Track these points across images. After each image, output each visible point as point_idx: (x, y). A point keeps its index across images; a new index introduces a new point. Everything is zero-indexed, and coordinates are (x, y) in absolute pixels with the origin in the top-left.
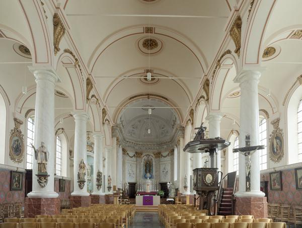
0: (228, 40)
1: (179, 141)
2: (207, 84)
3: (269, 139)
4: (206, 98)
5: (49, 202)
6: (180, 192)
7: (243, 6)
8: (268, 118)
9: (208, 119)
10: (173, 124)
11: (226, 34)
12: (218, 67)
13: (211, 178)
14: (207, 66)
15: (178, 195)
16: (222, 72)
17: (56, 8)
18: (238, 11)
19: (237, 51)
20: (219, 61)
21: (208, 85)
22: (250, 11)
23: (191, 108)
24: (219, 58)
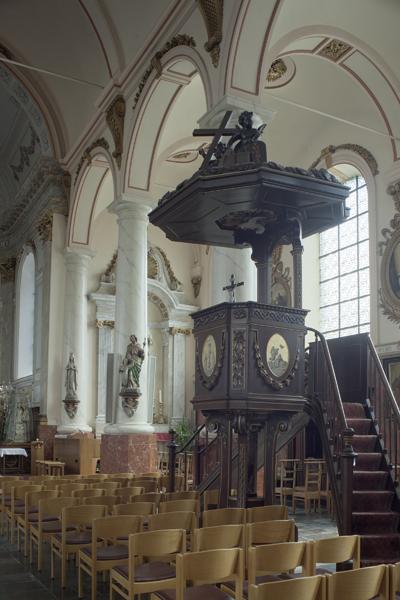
0: (189, 6)
1: (50, 222)
2: (116, 113)
3: (380, 244)
4: (112, 148)
6: (51, 422)
8: (375, 172)
9: (118, 212)
10: (17, 163)
12: (155, 72)
13: (285, 355)
14: (122, 67)
15: (41, 435)
16: (162, 89)
18: (120, 86)
20: (159, 56)
21: (122, 115)
22: (138, 95)
23: (115, 93)
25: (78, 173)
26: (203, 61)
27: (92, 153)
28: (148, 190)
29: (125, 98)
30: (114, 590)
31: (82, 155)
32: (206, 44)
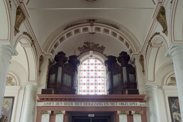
0: (156, 23)
5: (5, 118)
7: (150, 34)
11: (153, 20)
12: (150, 46)
17: (20, 3)
18: (161, 3)
19: (165, 31)
20: (150, 41)
24: (150, 39)
25: (146, 54)
26: (163, 38)
27: (151, 42)
28: (154, 81)
29: (164, 7)
30: (43, 49)
31: (147, 44)
32: (163, 31)
